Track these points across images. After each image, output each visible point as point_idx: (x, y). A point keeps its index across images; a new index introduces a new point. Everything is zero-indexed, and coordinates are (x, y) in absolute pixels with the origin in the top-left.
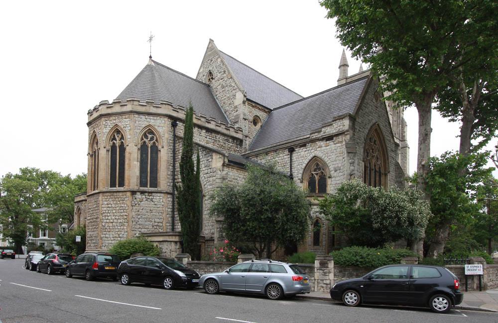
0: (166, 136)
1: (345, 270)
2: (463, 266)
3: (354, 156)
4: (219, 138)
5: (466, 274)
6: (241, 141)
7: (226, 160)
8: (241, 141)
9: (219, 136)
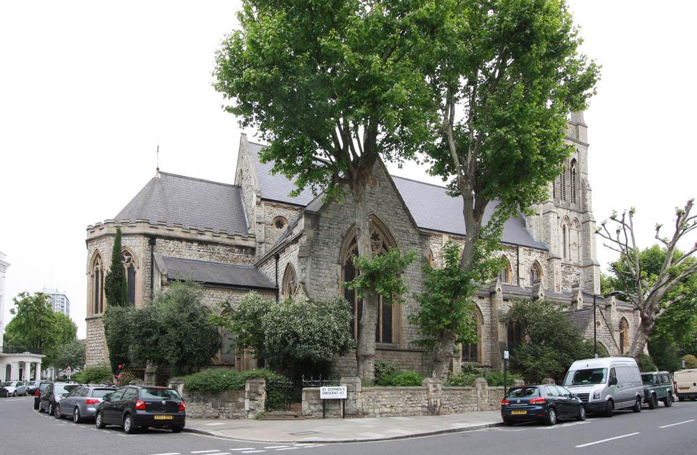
0: (142, 255)
1: (193, 395)
2: (318, 388)
3: (307, 260)
4: (218, 250)
5: (321, 398)
6: (253, 250)
7: (165, 279)
8: (253, 250)
9: (218, 247)
